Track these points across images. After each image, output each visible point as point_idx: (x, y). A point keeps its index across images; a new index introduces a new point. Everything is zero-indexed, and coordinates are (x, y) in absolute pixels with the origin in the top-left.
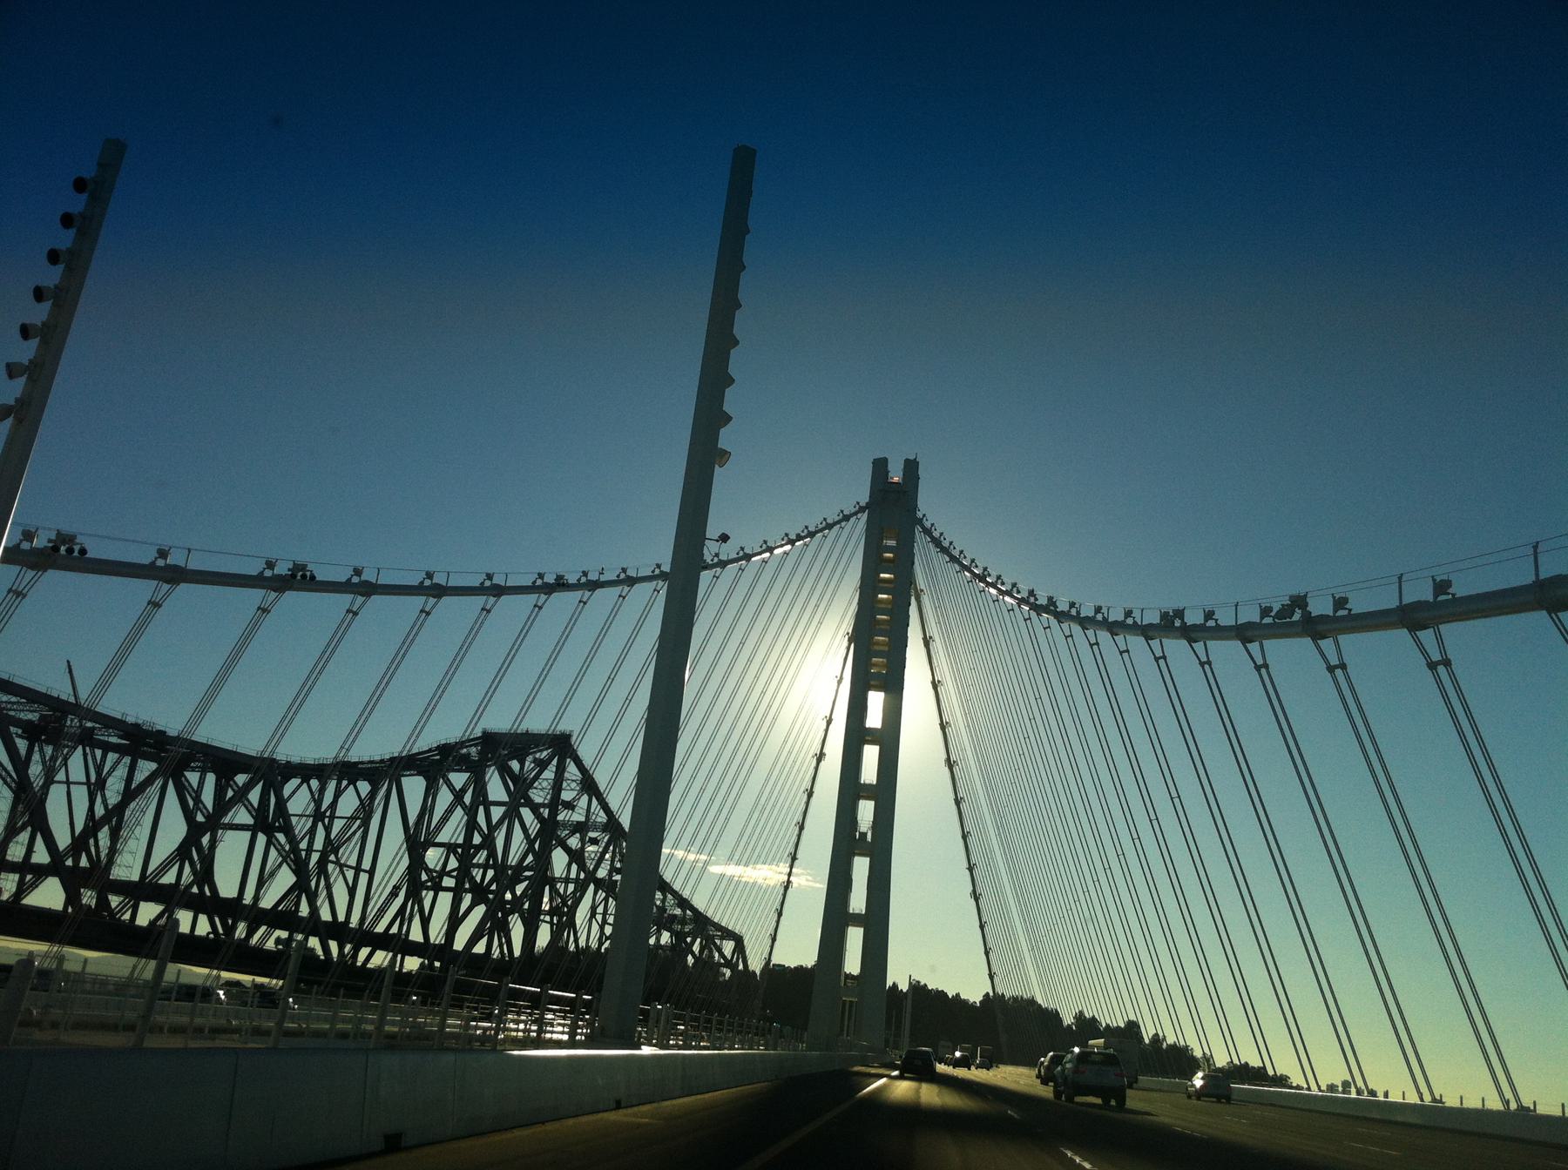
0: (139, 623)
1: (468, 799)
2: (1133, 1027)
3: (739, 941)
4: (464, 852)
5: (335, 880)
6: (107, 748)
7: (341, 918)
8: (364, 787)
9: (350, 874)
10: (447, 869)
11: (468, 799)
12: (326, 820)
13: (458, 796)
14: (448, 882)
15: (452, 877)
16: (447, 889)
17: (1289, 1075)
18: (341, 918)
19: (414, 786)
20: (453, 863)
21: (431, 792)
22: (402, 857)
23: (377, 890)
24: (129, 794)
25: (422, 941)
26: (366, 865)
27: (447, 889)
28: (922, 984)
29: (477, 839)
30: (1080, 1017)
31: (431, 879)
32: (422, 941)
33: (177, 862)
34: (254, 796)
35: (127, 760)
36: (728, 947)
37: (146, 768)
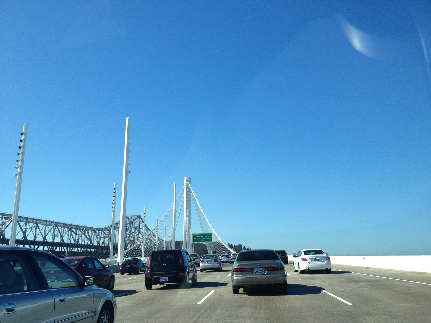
2: (240, 245)
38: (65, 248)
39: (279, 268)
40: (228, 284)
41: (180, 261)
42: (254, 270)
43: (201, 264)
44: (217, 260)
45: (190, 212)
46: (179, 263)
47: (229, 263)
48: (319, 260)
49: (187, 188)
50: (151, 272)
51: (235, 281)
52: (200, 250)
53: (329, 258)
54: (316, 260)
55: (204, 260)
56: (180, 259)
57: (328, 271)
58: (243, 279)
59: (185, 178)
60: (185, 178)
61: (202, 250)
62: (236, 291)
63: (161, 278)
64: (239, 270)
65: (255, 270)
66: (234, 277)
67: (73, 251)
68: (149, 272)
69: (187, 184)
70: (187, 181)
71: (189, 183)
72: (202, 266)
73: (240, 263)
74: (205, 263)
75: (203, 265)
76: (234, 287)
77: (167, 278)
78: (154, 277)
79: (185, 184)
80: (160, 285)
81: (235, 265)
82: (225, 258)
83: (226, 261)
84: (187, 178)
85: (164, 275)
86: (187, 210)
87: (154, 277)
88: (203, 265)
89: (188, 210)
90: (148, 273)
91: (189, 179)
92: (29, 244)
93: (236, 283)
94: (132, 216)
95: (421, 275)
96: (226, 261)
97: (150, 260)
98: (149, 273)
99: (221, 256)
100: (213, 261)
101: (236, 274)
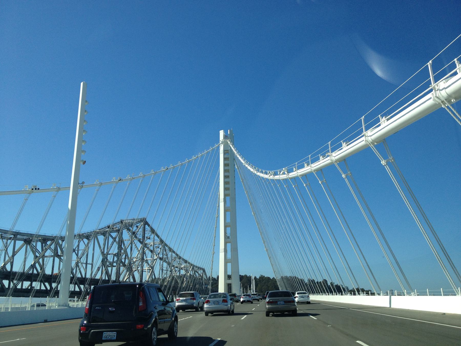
0: (13, 224)
1: (117, 240)
2: (325, 281)
3: (204, 271)
4: (118, 255)
5: (81, 267)
6: (8, 239)
7: (84, 276)
8: (86, 241)
9: (84, 265)
10: (114, 261)
11: (117, 240)
12: (76, 251)
13: (114, 239)
14: (115, 264)
15: (116, 263)
16: (115, 266)
17: (371, 290)
18: (84, 276)
19: (101, 238)
20: (116, 259)
21: (106, 239)
22: (100, 256)
23: (94, 265)
24: (14, 254)
25: (45, 289)
26: (90, 261)
27: (115, 266)
28: (263, 276)
29: (122, 251)
30: (309, 280)
31: (110, 264)
32: (45, 289)
33: (32, 269)
34: (53, 247)
35: (13, 241)
36: (200, 272)
37: (19, 243)
38: (47, 284)
39: (292, 302)
40: (227, 343)
41: (141, 304)
42: (278, 303)
43: (206, 306)
44: (226, 300)
45: (233, 200)
46: (139, 306)
47: (251, 303)
48: (303, 297)
49: (226, 152)
50: (89, 322)
51: (267, 308)
52: (269, 287)
53: (309, 296)
54: (302, 297)
55: (210, 300)
56: (141, 299)
57: (309, 303)
58: (272, 307)
59: (222, 133)
60: (222, 133)
61: (273, 286)
62: (268, 315)
63: (104, 333)
64: (270, 302)
65: (279, 303)
66: (267, 306)
67: (19, 287)
68: (85, 322)
69: (226, 145)
70: (225, 137)
71: (228, 141)
72: (207, 308)
73: (270, 298)
74: (210, 304)
75: (208, 306)
76: (267, 312)
77: (116, 333)
78: (92, 331)
79: (220, 142)
80: (211, 314)
81: (267, 300)
82: (246, 297)
83: (247, 301)
84: (226, 132)
85: (110, 327)
86: (227, 197)
87: (92, 331)
88: (208, 306)
89: (228, 198)
90: (84, 323)
91: (229, 133)
92: (44, 282)
93: (268, 309)
94: (130, 220)
95: (303, 299)
96: (247, 300)
97: (89, 300)
98: (85, 324)
99: (243, 296)
100: (221, 302)
101: (268, 305)
